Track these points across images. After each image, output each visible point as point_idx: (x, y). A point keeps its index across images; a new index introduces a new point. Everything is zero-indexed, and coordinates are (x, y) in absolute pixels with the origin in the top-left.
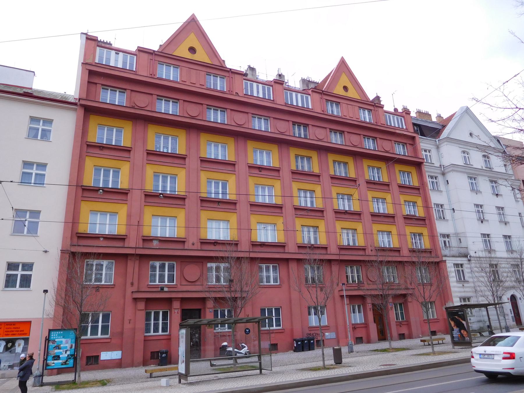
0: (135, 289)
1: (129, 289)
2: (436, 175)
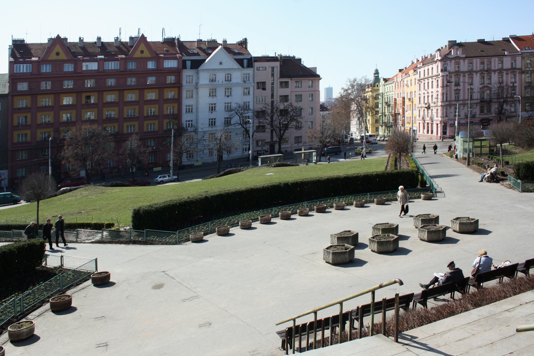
2: (215, 88)
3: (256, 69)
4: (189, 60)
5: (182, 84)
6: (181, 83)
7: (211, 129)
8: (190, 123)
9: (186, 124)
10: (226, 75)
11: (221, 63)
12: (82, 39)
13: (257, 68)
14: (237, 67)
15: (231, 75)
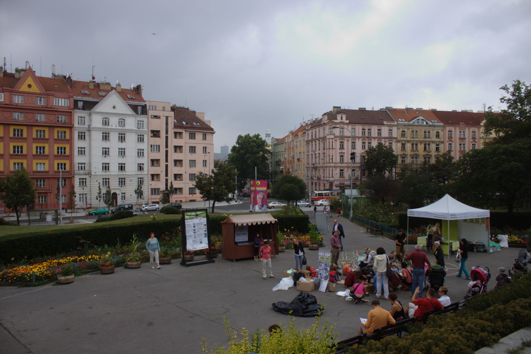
2: (84, 131)
3: (150, 117)
4: (81, 101)
5: (73, 125)
6: (72, 124)
7: (104, 173)
8: (83, 165)
9: (79, 166)
10: (103, 119)
11: (114, 107)
13: (151, 116)
14: (132, 114)
15: (108, 119)
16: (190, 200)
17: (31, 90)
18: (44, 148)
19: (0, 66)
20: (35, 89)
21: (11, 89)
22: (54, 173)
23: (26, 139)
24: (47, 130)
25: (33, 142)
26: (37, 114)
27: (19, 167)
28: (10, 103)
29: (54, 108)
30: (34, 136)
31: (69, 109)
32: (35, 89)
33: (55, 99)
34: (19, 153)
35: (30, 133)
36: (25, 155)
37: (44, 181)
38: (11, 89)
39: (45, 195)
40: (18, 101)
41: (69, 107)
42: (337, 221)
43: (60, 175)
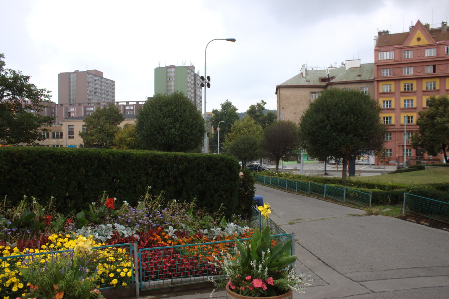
0: (399, 142)
1: (397, 142)
12: (445, 23)
16: (424, 169)
17: (421, 43)
18: (390, 101)
19: (1, 53)
20: (424, 41)
21: (401, 46)
22: (400, 127)
23: (439, 91)
24: (414, 83)
25: (401, 95)
26: (426, 67)
27: (385, 121)
28: (400, 60)
29: (403, 61)
30: (402, 89)
31: (394, 62)
32: (424, 41)
33: (379, 53)
34: (406, 106)
35: (420, 86)
36: (394, 109)
37: (390, 135)
38: (401, 46)
39: (410, 148)
40: (408, 56)
41: (394, 59)
42: (22, 297)
43: (406, 128)
